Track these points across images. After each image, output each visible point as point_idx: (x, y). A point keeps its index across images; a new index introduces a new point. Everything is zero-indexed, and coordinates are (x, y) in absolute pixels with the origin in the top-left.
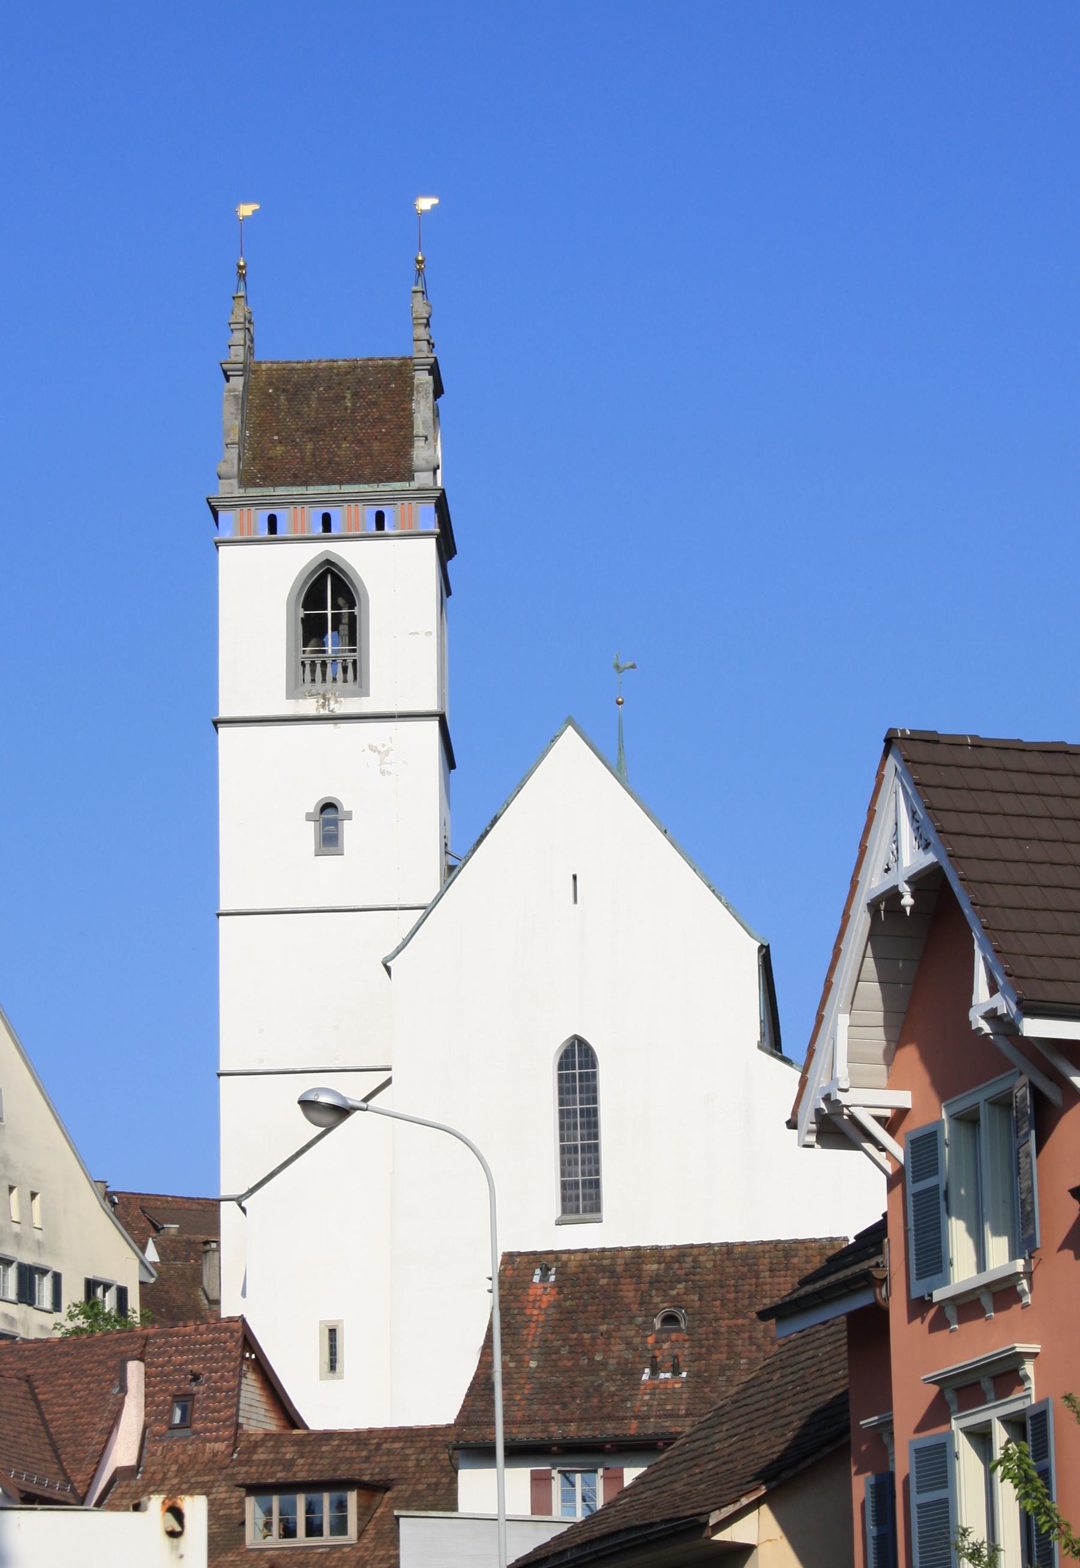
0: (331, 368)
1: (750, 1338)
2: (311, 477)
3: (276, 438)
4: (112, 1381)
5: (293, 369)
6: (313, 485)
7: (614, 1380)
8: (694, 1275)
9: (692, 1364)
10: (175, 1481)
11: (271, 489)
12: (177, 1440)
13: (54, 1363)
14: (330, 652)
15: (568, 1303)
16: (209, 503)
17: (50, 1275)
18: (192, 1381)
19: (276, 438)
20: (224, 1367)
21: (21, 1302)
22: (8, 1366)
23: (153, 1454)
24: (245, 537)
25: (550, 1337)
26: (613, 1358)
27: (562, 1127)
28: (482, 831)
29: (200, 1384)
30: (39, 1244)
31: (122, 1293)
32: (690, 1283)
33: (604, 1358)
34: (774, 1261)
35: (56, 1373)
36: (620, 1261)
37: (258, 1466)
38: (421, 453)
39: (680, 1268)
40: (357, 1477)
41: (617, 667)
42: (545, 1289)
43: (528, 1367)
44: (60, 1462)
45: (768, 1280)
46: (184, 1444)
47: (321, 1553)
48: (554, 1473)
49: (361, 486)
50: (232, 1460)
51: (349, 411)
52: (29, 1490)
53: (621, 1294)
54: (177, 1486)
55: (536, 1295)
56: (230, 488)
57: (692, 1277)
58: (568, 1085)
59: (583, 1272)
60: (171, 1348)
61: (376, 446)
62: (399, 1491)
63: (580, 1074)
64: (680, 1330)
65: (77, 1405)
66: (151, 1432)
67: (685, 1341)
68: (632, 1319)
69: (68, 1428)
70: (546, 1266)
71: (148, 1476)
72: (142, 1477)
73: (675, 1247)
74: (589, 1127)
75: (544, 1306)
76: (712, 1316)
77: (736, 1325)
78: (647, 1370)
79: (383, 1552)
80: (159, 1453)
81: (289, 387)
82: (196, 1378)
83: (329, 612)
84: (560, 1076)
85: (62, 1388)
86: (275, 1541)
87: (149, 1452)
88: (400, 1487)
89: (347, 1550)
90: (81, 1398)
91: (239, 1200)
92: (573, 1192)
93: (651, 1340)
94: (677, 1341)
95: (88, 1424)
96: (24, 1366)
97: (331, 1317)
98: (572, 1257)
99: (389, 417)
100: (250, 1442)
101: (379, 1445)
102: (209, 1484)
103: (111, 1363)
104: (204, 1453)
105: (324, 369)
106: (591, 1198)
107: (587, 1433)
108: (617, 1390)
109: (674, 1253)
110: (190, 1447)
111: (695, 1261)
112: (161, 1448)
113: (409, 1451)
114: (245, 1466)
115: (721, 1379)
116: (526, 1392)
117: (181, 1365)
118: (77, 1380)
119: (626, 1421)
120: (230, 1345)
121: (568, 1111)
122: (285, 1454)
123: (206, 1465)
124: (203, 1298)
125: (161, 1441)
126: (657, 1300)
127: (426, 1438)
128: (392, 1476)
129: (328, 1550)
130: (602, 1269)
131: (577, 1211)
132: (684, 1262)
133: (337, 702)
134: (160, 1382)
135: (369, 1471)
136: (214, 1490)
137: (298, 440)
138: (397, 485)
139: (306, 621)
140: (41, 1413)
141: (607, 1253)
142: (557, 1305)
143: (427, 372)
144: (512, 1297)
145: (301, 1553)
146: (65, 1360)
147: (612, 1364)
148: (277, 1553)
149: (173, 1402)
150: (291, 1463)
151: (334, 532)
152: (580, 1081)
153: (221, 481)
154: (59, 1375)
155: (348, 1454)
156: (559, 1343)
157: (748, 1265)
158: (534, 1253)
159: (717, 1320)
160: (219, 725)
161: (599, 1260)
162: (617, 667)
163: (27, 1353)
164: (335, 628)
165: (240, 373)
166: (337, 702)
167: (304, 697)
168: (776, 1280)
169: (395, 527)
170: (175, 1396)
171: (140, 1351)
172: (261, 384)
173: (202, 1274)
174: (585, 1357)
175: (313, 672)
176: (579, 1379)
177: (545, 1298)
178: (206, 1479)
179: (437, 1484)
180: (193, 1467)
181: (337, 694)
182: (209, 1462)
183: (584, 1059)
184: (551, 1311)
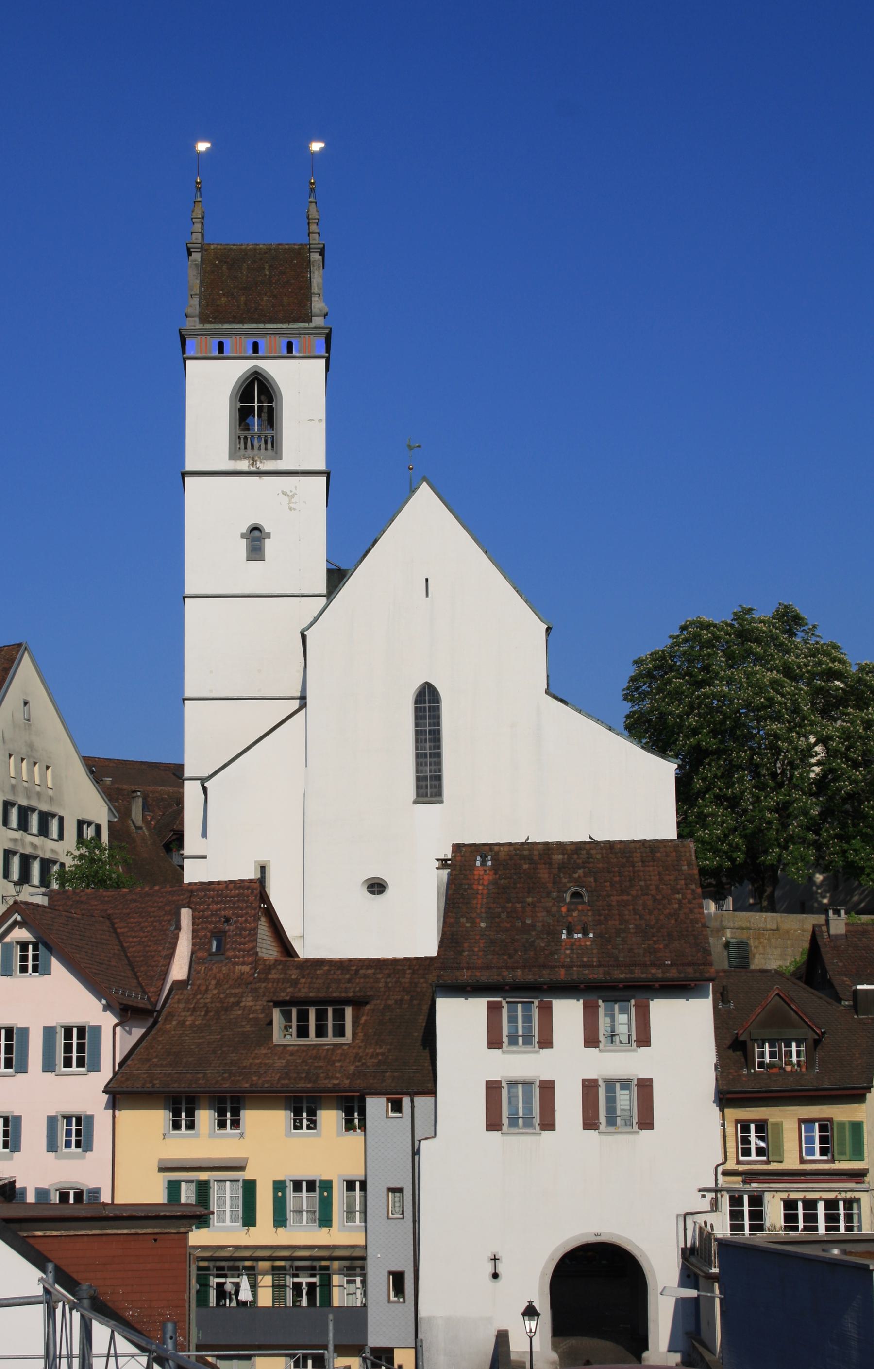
0: (255, 249)
1: (634, 909)
2: (245, 318)
3: (221, 292)
4: (169, 921)
5: (231, 249)
6: (246, 323)
7: (543, 939)
8: (589, 863)
9: (595, 927)
10: (215, 992)
11: (220, 325)
12: (215, 963)
13: (126, 906)
14: (256, 431)
15: (502, 881)
16: (180, 333)
17: (57, 817)
18: (225, 922)
19: (221, 292)
20: (247, 913)
21: (41, 835)
22: (94, 907)
23: (199, 972)
24: (204, 355)
25: (493, 906)
26: (539, 922)
27: (417, 741)
28: (366, 549)
29: (231, 925)
30: (51, 798)
31: (98, 828)
32: (587, 869)
33: (532, 922)
34: (644, 855)
35: (129, 914)
36: (536, 852)
37: (273, 983)
38: (318, 304)
39: (579, 858)
40: (343, 995)
41: (409, 446)
42: (485, 871)
43: (480, 927)
44: (137, 978)
45: (642, 868)
46: (220, 965)
47: (328, 1050)
48: (504, 1003)
49: (278, 325)
50: (255, 978)
51: (267, 277)
52: (125, 1002)
53: (539, 876)
54: (217, 995)
55: (479, 875)
56: (193, 323)
57: (588, 865)
58: (421, 714)
59: (511, 859)
60: (209, 899)
61: (285, 300)
62: (375, 1005)
63: (429, 707)
64: (583, 903)
65: (146, 937)
66: (196, 957)
67: (588, 910)
68: (548, 894)
69: (140, 953)
70: (485, 855)
71: (196, 987)
72: (191, 988)
73: (573, 843)
74: (434, 741)
75: (486, 883)
76: (605, 893)
77: (622, 900)
78: (564, 932)
79: (371, 1051)
80: (202, 972)
81: (228, 260)
82: (227, 920)
83: (256, 405)
84: (416, 708)
85: (134, 924)
86: (292, 1039)
87: (195, 971)
88: (375, 1002)
89: (346, 1047)
90: (148, 932)
91: (203, 780)
92: (424, 783)
93: (564, 909)
94: (583, 911)
95: (155, 951)
96: (105, 908)
97: (262, 858)
98: (502, 849)
99: (293, 281)
100: (266, 965)
101: (357, 971)
102: (240, 995)
103: (167, 908)
104: (234, 973)
105: (250, 250)
106: (435, 787)
107: (530, 977)
108: (546, 946)
109: (573, 847)
110: (224, 968)
111: (588, 853)
112: (203, 968)
113: (380, 976)
114: (263, 982)
115: (618, 939)
116: (482, 945)
117: (216, 911)
118: (144, 919)
119: (557, 969)
120: (251, 898)
121: (421, 731)
122: (291, 975)
123: (236, 981)
124: (132, 825)
125: (203, 963)
126: (565, 880)
127: (390, 967)
128: (369, 993)
129: (332, 1047)
130: (523, 858)
131: (427, 795)
132: (581, 854)
133: (261, 463)
134: (202, 922)
135: (352, 990)
136: (244, 999)
137: (235, 294)
138: (302, 325)
139: (241, 410)
140: (120, 942)
141: (525, 846)
142: (495, 883)
143: (318, 254)
144: (462, 876)
145: (313, 1049)
146: (134, 905)
147: (539, 927)
148: (296, 1048)
149: (211, 937)
150: (295, 982)
151: (260, 354)
152: (429, 711)
153: (188, 319)
154: (131, 915)
155: (335, 977)
156: (500, 910)
157: (626, 857)
158: (475, 845)
159: (609, 896)
160: (185, 475)
161: (521, 851)
162: (409, 446)
163: (106, 898)
164: (259, 416)
165: (199, 250)
166: (261, 463)
167: (240, 458)
168: (647, 868)
169: (299, 352)
170: (212, 932)
171: (188, 900)
172: (211, 258)
173: (131, 811)
174: (519, 921)
175: (246, 443)
176: (517, 937)
177: (486, 877)
178: (237, 991)
179: (401, 1000)
180: (227, 982)
181: (261, 457)
182: (238, 979)
183: (431, 697)
184: (491, 887)
